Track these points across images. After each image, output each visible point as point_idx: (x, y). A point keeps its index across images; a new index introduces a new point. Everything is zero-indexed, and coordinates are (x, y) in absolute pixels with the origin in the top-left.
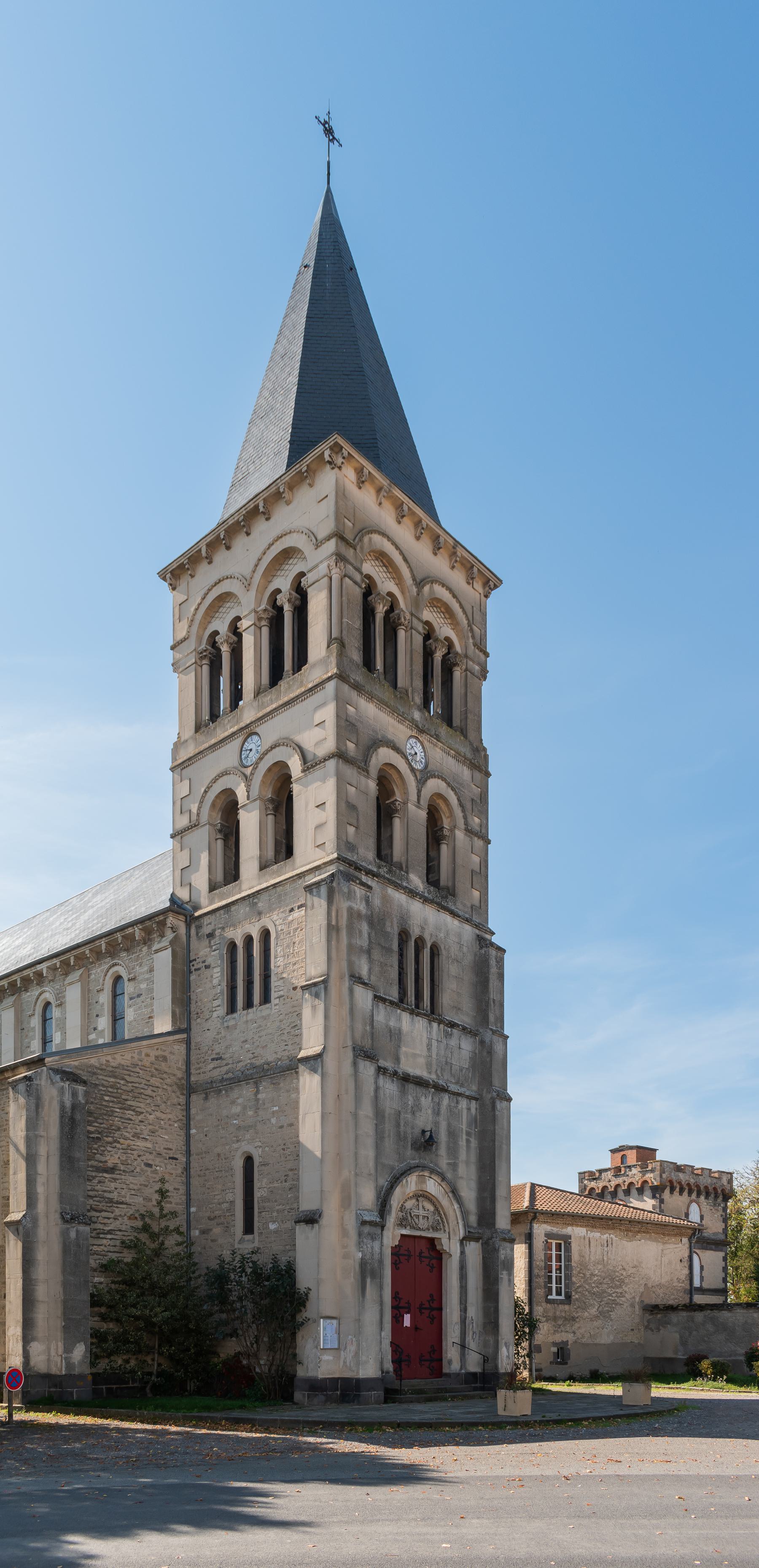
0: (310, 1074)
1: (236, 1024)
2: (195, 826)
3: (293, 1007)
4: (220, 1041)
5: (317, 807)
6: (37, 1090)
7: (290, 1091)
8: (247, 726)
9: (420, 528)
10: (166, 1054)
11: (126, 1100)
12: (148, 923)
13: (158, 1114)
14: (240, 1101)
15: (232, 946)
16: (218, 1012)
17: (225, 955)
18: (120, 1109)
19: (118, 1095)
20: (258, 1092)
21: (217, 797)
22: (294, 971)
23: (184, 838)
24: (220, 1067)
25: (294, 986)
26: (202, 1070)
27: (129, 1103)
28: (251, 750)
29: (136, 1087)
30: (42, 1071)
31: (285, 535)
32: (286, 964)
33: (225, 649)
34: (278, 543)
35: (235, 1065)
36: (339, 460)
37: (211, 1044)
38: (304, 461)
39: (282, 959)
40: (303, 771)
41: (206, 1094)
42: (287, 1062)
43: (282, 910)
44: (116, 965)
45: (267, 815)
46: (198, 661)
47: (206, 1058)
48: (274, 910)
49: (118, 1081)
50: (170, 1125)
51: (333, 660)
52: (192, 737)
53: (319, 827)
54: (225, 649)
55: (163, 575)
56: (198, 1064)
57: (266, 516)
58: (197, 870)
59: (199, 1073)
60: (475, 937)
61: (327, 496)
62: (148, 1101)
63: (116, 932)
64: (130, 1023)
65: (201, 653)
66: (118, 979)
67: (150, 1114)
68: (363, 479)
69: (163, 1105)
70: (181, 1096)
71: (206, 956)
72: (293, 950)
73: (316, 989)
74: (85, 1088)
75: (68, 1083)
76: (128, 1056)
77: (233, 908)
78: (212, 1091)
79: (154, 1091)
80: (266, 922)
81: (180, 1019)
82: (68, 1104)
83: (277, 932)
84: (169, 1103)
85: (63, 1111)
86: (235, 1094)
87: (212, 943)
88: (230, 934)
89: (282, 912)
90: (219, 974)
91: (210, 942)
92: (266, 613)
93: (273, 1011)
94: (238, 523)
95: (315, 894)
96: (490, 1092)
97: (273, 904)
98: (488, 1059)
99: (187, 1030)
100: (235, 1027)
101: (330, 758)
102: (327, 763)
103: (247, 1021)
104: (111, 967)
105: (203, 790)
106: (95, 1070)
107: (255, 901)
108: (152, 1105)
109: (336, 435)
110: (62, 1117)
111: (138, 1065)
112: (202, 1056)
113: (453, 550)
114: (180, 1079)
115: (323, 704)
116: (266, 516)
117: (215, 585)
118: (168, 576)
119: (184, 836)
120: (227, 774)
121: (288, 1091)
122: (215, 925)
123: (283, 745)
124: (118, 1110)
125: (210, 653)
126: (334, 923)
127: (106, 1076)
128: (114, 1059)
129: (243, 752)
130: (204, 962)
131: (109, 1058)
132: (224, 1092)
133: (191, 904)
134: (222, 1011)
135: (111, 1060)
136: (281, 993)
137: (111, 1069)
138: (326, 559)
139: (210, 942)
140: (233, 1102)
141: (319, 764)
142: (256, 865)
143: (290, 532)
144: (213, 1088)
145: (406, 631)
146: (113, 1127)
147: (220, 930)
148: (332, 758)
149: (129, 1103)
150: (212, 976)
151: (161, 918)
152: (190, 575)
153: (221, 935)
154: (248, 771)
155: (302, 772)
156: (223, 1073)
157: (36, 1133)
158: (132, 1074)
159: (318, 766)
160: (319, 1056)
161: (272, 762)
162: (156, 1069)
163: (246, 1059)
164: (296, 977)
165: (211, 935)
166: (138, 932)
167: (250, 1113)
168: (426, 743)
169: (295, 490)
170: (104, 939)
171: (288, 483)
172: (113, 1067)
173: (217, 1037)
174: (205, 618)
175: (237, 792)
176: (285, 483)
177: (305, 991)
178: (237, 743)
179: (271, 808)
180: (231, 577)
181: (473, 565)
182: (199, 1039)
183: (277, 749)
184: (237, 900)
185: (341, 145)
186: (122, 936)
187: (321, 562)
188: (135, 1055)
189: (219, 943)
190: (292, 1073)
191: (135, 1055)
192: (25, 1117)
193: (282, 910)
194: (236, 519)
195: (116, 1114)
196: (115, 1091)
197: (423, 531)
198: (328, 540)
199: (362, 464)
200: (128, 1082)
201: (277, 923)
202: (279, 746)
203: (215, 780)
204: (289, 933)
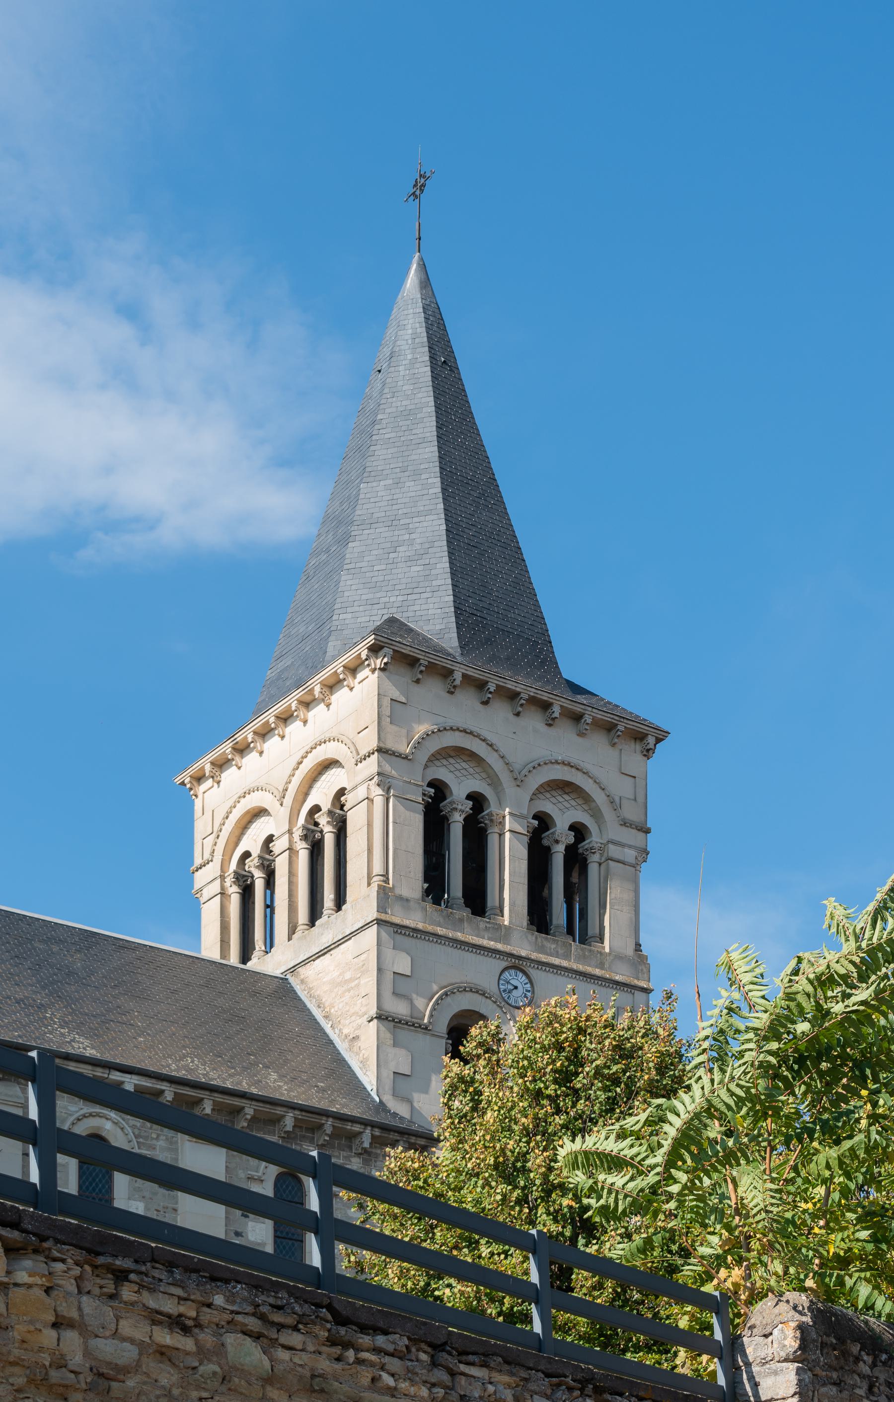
8: (520, 958)
28: (516, 988)
31: (578, 769)
34: (566, 768)
38: (625, 721)
119: (399, 1028)
120: (483, 995)
170: (297, 1112)
194: (518, 689)
198: (639, 830)
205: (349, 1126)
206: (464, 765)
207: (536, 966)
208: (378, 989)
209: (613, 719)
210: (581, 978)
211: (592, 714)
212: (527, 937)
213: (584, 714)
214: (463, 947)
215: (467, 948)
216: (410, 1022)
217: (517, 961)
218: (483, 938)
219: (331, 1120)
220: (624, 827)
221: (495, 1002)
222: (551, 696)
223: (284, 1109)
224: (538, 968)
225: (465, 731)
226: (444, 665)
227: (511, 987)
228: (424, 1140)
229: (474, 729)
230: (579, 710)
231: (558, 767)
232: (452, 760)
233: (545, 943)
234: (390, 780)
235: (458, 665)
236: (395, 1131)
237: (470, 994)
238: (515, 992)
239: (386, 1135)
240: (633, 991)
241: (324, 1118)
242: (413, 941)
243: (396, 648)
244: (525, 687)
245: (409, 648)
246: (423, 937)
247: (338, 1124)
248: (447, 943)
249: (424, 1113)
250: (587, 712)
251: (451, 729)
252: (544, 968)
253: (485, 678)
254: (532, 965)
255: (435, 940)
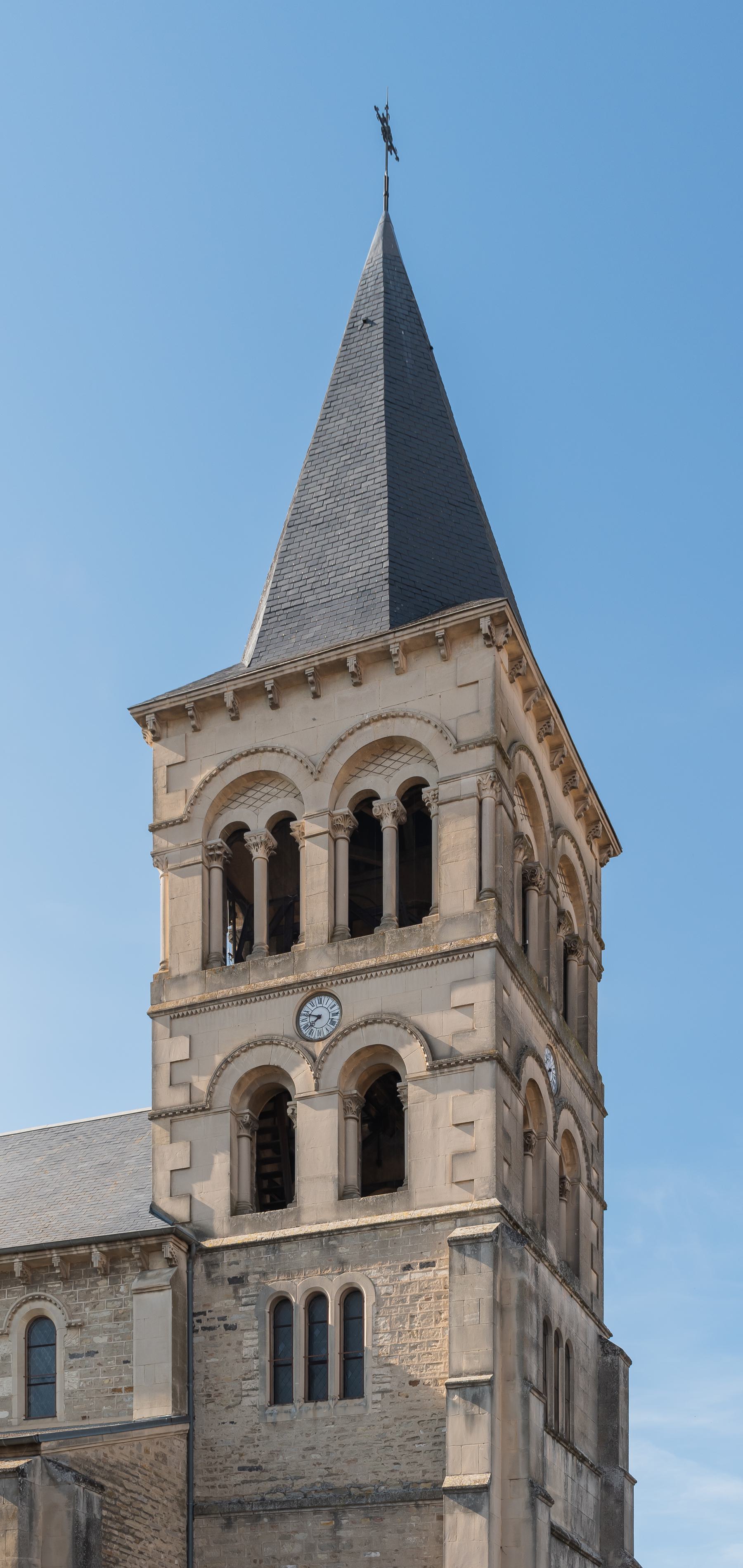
0: (465, 1512)
1: (293, 1421)
2: (204, 1109)
3: (411, 1409)
4: (257, 1442)
5: (457, 1125)
6: (31, 1491)
7: (404, 1531)
8: (315, 981)
9: (559, 754)
10: (165, 1451)
11: (125, 1518)
12: (122, 1246)
13: (158, 1542)
14: (300, 1536)
15: (282, 1303)
16: (252, 1399)
17: (268, 1315)
18: (119, 1530)
19: (117, 1509)
20: (338, 1526)
21: (248, 1074)
22: (412, 1357)
23: (175, 1124)
24: (259, 1482)
25: (413, 1379)
26: (218, 1483)
27: (127, 1522)
28: (319, 1017)
29: (136, 1500)
30: (36, 1461)
31: (393, 717)
32: (396, 1345)
33: (260, 857)
34: (379, 724)
35: (290, 1482)
36: (500, 638)
37: (238, 1444)
38: (442, 622)
39: (387, 1337)
40: (431, 1069)
41: (229, 1519)
42: (399, 1489)
43: (388, 1264)
44: (45, 1299)
45: (346, 1119)
46: (205, 860)
47: (228, 1464)
48: (374, 1262)
49: (117, 1487)
50: (170, 1561)
51: (490, 920)
52: (195, 974)
53: (459, 1155)
54: (260, 857)
55: (140, 715)
56: (210, 1472)
57: (355, 680)
58: (206, 1176)
59: (213, 1487)
60: (596, 1337)
61: (477, 682)
62: (147, 1523)
63: (50, 1249)
64: (70, 1394)
65: (212, 850)
66: (39, 1322)
67: (150, 1543)
68: (521, 671)
69: (164, 1529)
70: (181, 1518)
71: (228, 1311)
72: (411, 1327)
73: (476, 1390)
74: (100, 1496)
75: (83, 1485)
76: (127, 1450)
77: (285, 1247)
78: (244, 1517)
79: (154, 1508)
80: (355, 1276)
81: (181, 1401)
82: (83, 1520)
83: (377, 1295)
84: (169, 1528)
85: (77, 1528)
86: (290, 1524)
87: (241, 1292)
88: (278, 1284)
89: (389, 1268)
90: (256, 1341)
91: (236, 1291)
92: (348, 821)
93: (370, 1411)
94: (302, 675)
95: (468, 1252)
96: (620, 1557)
97: (370, 1253)
98: (617, 1511)
99: (189, 1418)
100: (290, 1425)
101: (483, 1059)
102: (477, 1066)
103: (315, 1420)
104: (27, 1301)
105: (219, 1059)
106: (92, 1468)
107: (331, 1243)
108: (152, 1528)
109: (505, 603)
110: (76, 1538)
111: (136, 1465)
112: (219, 1460)
113: (583, 793)
114: (180, 1492)
115: (471, 980)
116: (355, 680)
117: (246, 755)
118: (150, 718)
119: (177, 1120)
120: (271, 1043)
121: (400, 1532)
122: (247, 1267)
123: (391, 1022)
124: (116, 1532)
125: (225, 853)
126: (498, 1299)
127: (103, 1478)
128: (112, 1452)
129: (302, 1018)
130: (223, 1319)
131: (107, 1450)
132: (266, 1520)
133: (191, 1226)
134: (263, 1397)
135: (109, 1455)
136: (387, 1386)
137: (108, 1468)
138: (474, 772)
139: (236, 1291)
140: (285, 1537)
141: (462, 1065)
142: (330, 1191)
143: (404, 716)
144: (245, 1511)
145: (539, 895)
146: (112, 1559)
147: (257, 1276)
148: (487, 1060)
149: (127, 1522)
150: (240, 1343)
151: (153, 1241)
152: (194, 727)
153: (259, 1283)
154: (318, 1048)
155: (428, 1070)
156: (265, 1491)
157: (30, 1559)
158: (131, 1478)
159: (459, 1067)
160: (482, 1490)
161: (365, 1044)
162: (156, 1475)
163: (315, 1476)
164: (417, 1366)
165: (238, 1281)
166: (97, 1257)
167: (323, 1557)
168: (559, 1059)
169: (412, 656)
170: (21, 1256)
171: (405, 644)
172: (111, 1466)
173: (250, 1435)
174: (220, 799)
175: (293, 1075)
176: (400, 642)
177: (452, 1392)
178: (293, 1001)
179: (354, 1110)
180: (281, 751)
181: (600, 820)
182: (211, 1435)
183: (376, 1026)
184: (295, 1237)
185: (397, 159)
186: (62, 1257)
187: (467, 774)
188: (134, 1450)
189: (257, 1295)
190: (408, 1506)
191: (134, 1450)
192: (16, 1532)
193: (388, 1264)
194: (299, 669)
195: (114, 1539)
196: (113, 1503)
197: (562, 759)
198: (480, 746)
199: (522, 650)
200: (126, 1490)
201: (378, 1282)
202: (382, 1022)
203: (248, 1048)
204: (404, 1301)
205: (74, 1252)
206: (266, 790)
207: (339, 981)
208: (153, 1088)
209: (424, 629)
210: (399, 969)
211: (397, 640)
212: (326, 953)
213: (389, 646)
214: (248, 1000)
215: (253, 999)
216: (192, 1108)
217: (314, 986)
218: (272, 978)
219: (54, 1251)
220: (460, 755)
221: (286, 1046)
222: (339, 651)
223: (8, 1257)
224: (342, 982)
225: (249, 753)
226: (211, 694)
227: (313, 1019)
228: (154, 1238)
229: (257, 745)
230: (380, 645)
231: (369, 728)
232: (250, 793)
233: (349, 948)
234: (166, 855)
235: (224, 685)
236: (120, 1240)
237: (258, 1048)
238: (319, 1024)
239: (114, 1247)
240: (471, 954)
241: (47, 1252)
242: (193, 1019)
243: (156, 710)
244: (305, 661)
245: (168, 701)
246: (203, 1009)
247: (64, 1254)
248: (230, 1004)
249: (206, 1203)
250: (389, 642)
251: (341, 740)
252: (349, 979)
253: (258, 680)
254: (334, 982)
255: (216, 1006)
